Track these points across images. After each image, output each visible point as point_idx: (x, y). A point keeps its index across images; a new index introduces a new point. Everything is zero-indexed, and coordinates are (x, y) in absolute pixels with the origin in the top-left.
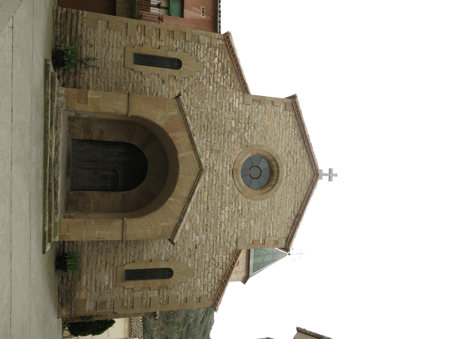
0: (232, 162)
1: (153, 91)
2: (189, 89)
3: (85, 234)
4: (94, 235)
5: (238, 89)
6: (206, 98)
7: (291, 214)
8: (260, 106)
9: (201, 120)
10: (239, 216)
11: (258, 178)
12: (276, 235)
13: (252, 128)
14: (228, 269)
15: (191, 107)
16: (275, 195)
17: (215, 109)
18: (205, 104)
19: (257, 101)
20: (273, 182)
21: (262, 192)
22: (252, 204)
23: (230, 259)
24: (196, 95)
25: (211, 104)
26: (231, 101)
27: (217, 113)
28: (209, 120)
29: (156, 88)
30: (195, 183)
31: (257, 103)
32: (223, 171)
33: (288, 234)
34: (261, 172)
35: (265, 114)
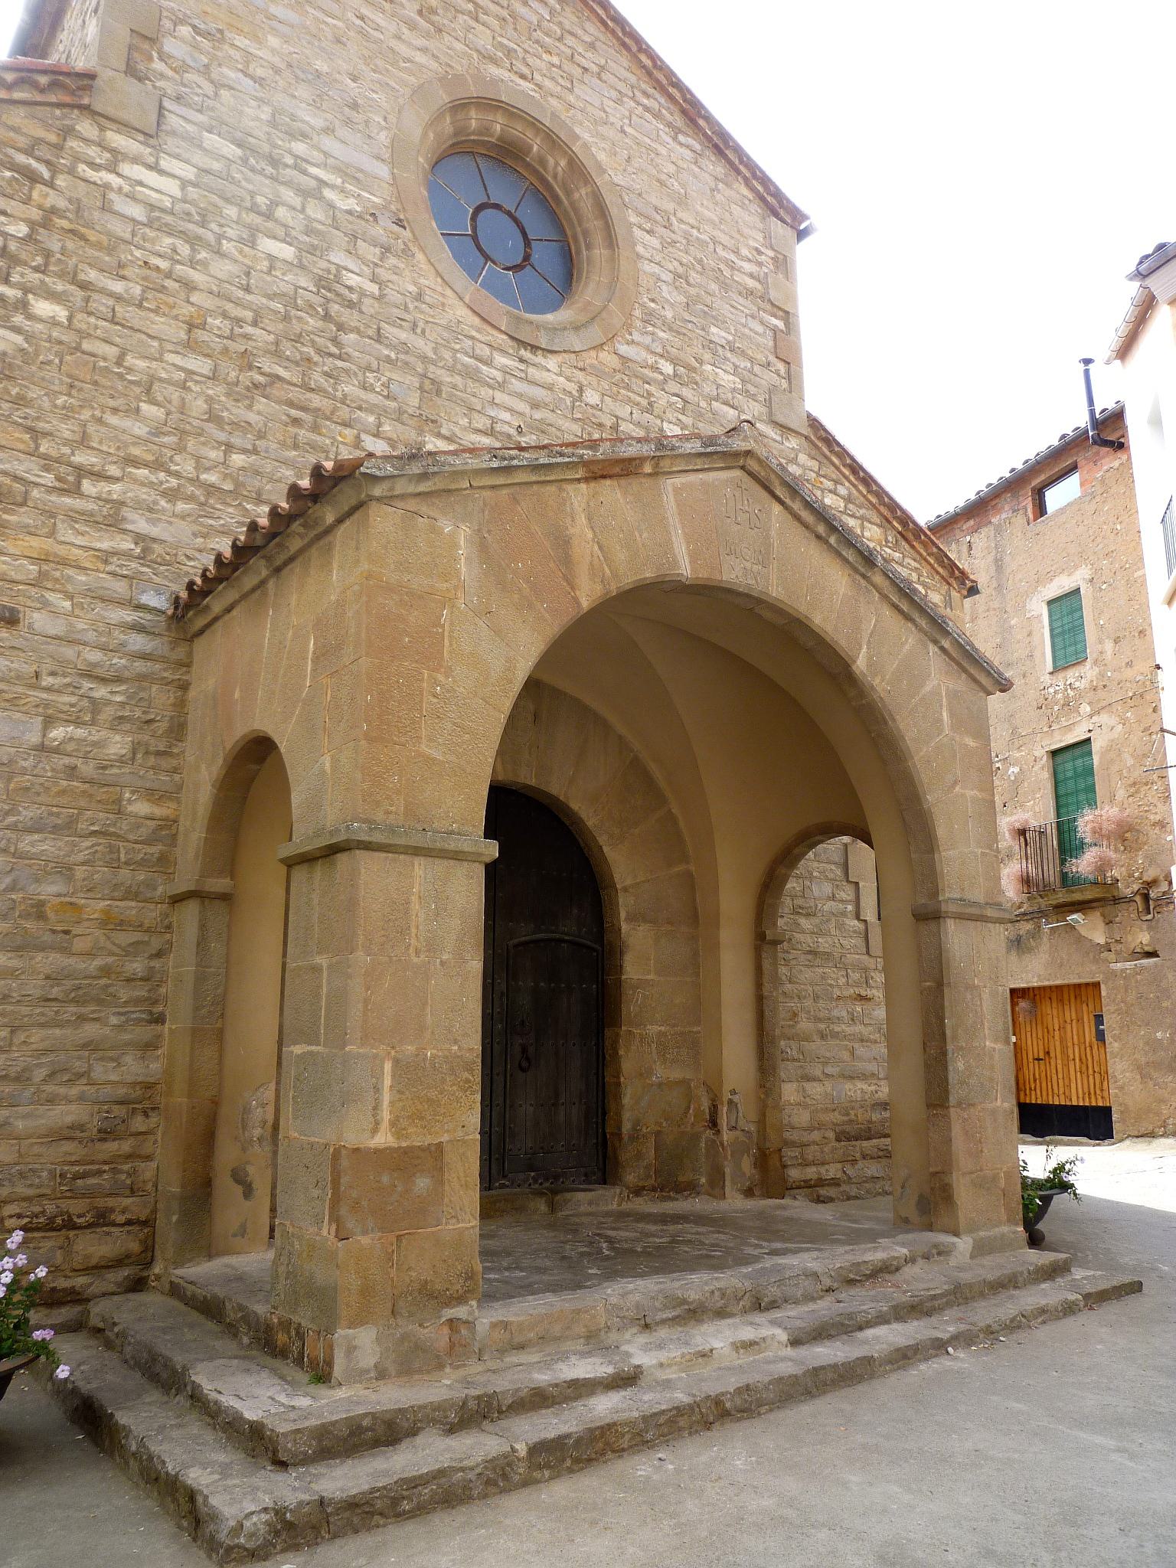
0: (478, 330)
1: (73, 699)
2: (54, 453)
3: (999, 1103)
4: (997, 1056)
5: (52, 138)
6: (119, 364)
7: (681, 144)
8: (169, 45)
9: (261, 435)
10: (696, 383)
11: (475, 238)
12: (757, 249)
13: (300, 147)
14: (864, 496)
15: (177, 475)
16: (616, 180)
17: (191, 326)
18: (161, 380)
19: (137, 49)
20: (557, 164)
21: (598, 238)
22: (653, 305)
23: (834, 477)
24: (100, 421)
25: (155, 344)
26: (137, 212)
27: (217, 322)
28: (256, 386)
29: (53, 674)
30: (797, 517)
31: (150, 59)
32: (520, 396)
33: (750, 196)
34: (497, 206)
35: (222, 40)
